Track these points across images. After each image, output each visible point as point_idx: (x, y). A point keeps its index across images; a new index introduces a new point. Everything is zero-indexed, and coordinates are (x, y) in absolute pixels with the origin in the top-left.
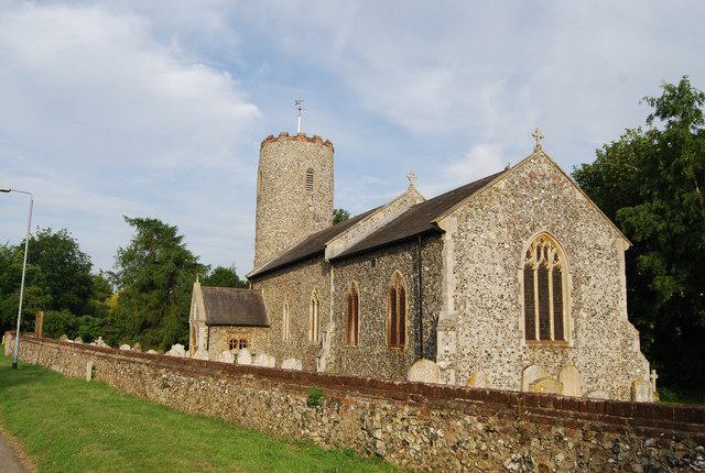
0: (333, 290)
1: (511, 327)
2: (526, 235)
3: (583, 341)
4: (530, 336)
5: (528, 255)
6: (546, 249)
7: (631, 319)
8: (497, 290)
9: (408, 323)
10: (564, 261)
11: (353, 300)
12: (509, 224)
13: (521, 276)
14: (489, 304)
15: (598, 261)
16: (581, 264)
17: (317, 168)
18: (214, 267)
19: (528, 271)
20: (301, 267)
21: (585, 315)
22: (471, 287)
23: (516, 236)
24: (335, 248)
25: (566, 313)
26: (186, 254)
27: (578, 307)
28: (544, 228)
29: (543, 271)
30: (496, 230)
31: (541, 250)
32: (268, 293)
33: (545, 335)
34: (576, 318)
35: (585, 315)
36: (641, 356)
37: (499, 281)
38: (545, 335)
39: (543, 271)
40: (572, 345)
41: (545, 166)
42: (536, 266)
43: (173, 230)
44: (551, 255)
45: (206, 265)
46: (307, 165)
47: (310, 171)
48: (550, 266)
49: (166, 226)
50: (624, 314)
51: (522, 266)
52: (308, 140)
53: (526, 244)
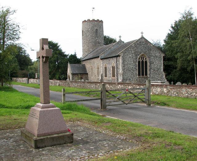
0: (102, 65)
1: (135, 73)
2: (139, 55)
3: (152, 76)
4: (139, 75)
5: (139, 59)
6: (143, 57)
7: (164, 71)
8: (131, 67)
9: (115, 73)
10: (148, 60)
11: (106, 68)
12: (134, 53)
13: (137, 63)
14: (130, 69)
15: (156, 59)
16: (152, 60)
17: (98, 29)
18: (70, 55)
19: (139, 62)
20: (95, 59)
21: (152, 71)
22: (126, 66)
23: (136, 55)
24: (102, 56)
25: (148, 70)
26: (60, 51)
27: (150, 69)
28: (143, 53)
29: (143, 62)
30: (131, 54)
31: (142, 57)
32: (88, 65)
33: (143, 75)
34: (150, 71)
35: (152, 71)
36: (165, 79)
37: (132, 65)
38: (143, 75)
39: (143, 62)
40: (149, 76)
41: (143, 40)
42: (141, 61)
43: (47, 39)
44: (144, 59)
45: (67, 54)
46: (96, 28)
47: (97, 30)
48: (144, 61)
49: (64, 53)
50: (162, 70)
51: (138, 61)
52: (96, 21)
53: (138, 57)
